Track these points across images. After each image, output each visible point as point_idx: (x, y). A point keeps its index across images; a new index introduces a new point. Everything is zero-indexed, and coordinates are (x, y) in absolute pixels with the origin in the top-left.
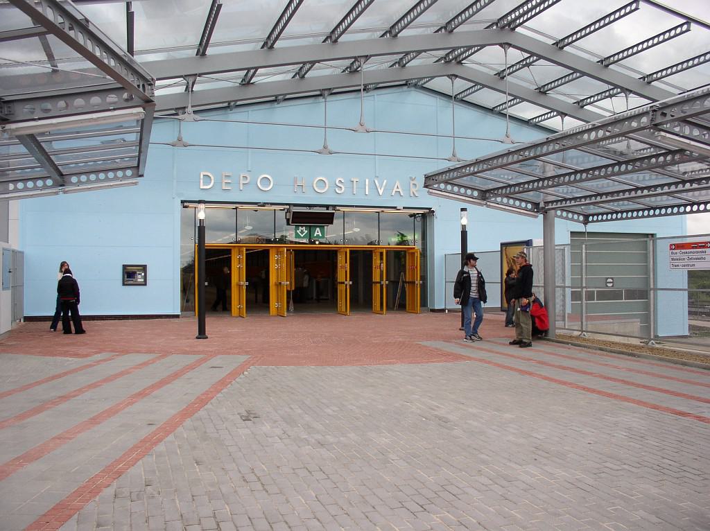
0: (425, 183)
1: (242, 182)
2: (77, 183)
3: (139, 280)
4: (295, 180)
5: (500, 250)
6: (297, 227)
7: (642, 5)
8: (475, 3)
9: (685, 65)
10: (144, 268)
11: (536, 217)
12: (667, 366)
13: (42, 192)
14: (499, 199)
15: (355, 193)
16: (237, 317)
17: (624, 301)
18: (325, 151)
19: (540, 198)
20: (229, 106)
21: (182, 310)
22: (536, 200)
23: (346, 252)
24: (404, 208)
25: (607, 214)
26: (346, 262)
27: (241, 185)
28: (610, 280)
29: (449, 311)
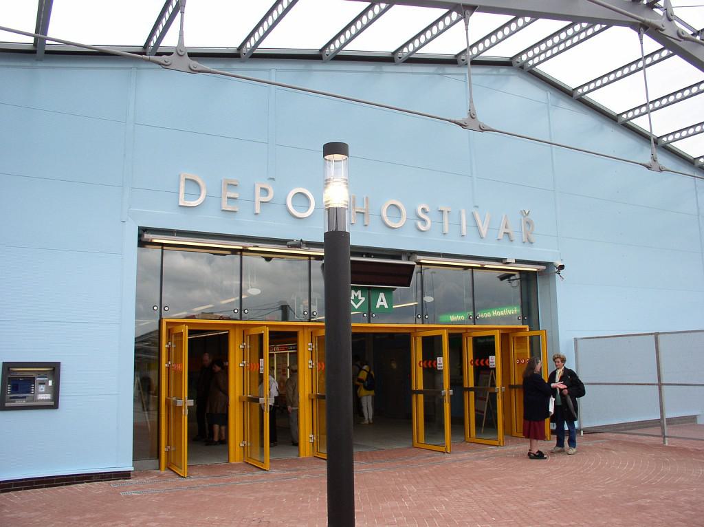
3: (41, 397)
9: (672, 99)
10: (54, 370)
15: (446, 231)
21: (137, 455)
24: (518, 261)
27: (258, 206)
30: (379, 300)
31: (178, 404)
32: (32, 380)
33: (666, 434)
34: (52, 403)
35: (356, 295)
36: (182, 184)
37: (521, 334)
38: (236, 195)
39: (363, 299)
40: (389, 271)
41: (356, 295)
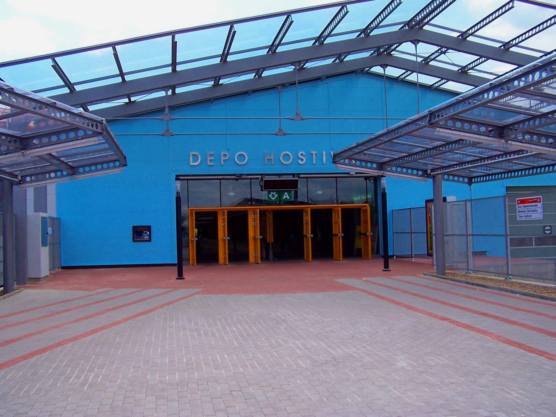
1: (223, 158)
3: (146, 237)
6: (269, 193)
10: (149, 228)
12: (493, 293)
16: (223, 264)
17: (534, 247)
18: (281, 133)
19: (430, 163)
20: (209, 101)
22: (425, 168)
25: (525, 170)
27: (222, 161)
29: (397, 257)
32: (142, 232)
33: (510, 273)
39: (273, 199)
40: (288, 184)
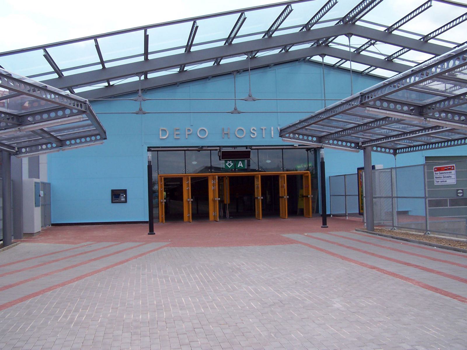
0: (280, 134)
2: (69, 145)
4: (223, 130)
5: (357, 173)
7: (434, 3)
8: (363, 2)
10: (125, 191)
11: (358, 152)
13: (95, 143)
14: (331, 142)
16: (187, 222)
17: (449, 207)
18: (236, 111)
19: (361, 137)
22: (357, 141)
23: (284, 177)
26: (285, 183)
28: (461, 191)
29: (333, 216)
30: (239, 164)
31: (215, 200)
32: (120, 195)
34: (125, 201)
35: (229, 163)
36: (160, 132)
37: (306, 175)
38: (179, 133)
39: (232, 164)
41: (229, 163)
